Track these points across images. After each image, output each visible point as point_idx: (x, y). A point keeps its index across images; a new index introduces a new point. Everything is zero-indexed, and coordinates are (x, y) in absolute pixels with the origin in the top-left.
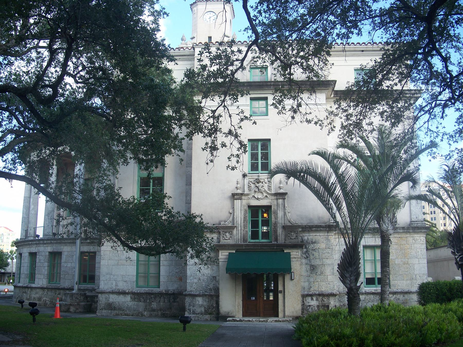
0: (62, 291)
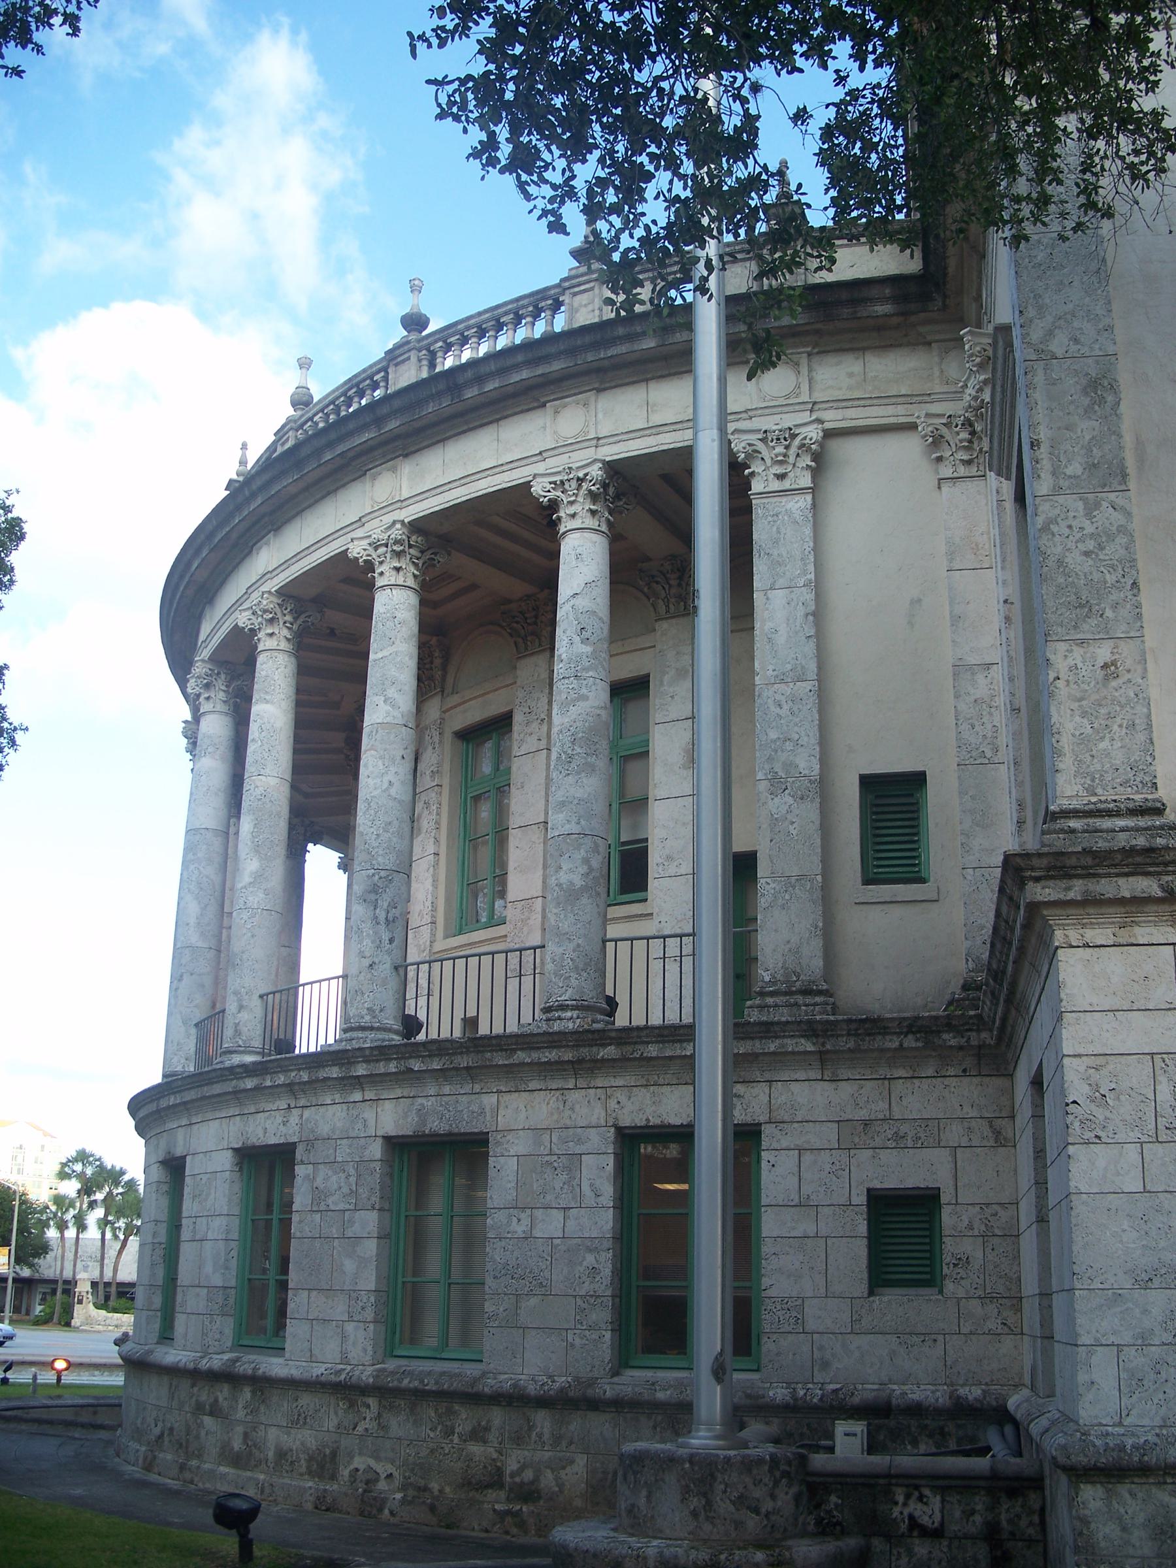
0: (497, 1417)
